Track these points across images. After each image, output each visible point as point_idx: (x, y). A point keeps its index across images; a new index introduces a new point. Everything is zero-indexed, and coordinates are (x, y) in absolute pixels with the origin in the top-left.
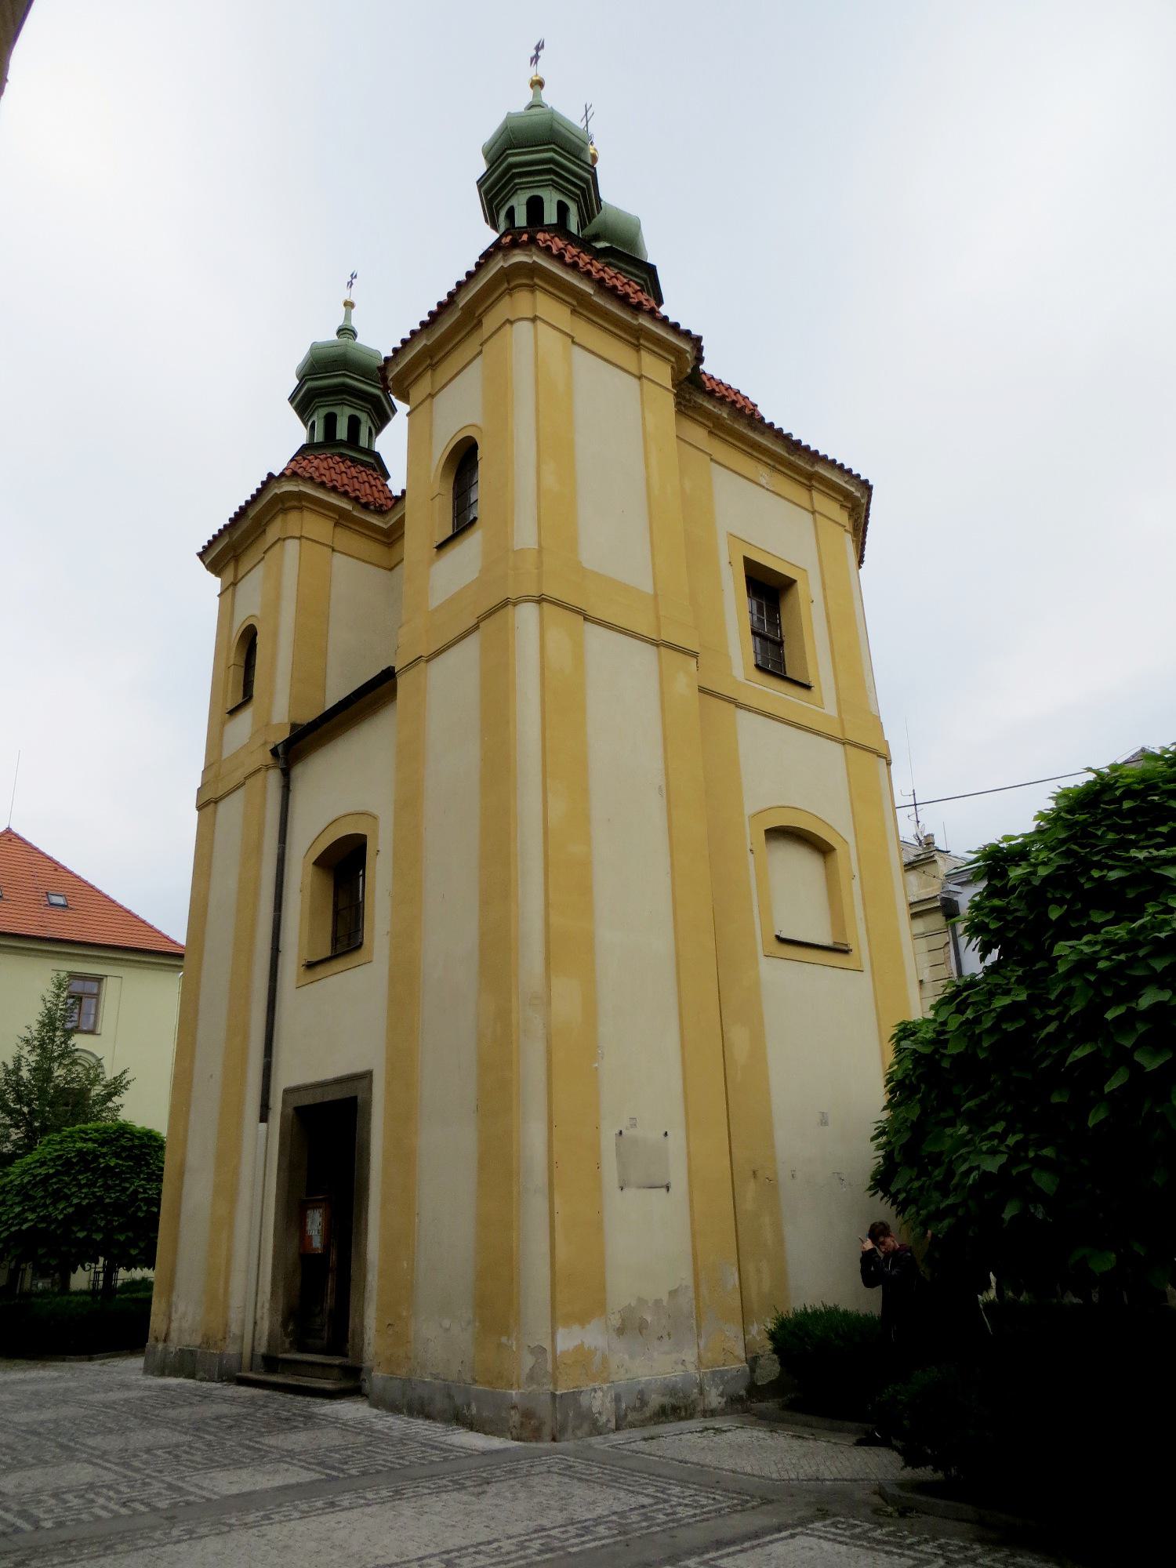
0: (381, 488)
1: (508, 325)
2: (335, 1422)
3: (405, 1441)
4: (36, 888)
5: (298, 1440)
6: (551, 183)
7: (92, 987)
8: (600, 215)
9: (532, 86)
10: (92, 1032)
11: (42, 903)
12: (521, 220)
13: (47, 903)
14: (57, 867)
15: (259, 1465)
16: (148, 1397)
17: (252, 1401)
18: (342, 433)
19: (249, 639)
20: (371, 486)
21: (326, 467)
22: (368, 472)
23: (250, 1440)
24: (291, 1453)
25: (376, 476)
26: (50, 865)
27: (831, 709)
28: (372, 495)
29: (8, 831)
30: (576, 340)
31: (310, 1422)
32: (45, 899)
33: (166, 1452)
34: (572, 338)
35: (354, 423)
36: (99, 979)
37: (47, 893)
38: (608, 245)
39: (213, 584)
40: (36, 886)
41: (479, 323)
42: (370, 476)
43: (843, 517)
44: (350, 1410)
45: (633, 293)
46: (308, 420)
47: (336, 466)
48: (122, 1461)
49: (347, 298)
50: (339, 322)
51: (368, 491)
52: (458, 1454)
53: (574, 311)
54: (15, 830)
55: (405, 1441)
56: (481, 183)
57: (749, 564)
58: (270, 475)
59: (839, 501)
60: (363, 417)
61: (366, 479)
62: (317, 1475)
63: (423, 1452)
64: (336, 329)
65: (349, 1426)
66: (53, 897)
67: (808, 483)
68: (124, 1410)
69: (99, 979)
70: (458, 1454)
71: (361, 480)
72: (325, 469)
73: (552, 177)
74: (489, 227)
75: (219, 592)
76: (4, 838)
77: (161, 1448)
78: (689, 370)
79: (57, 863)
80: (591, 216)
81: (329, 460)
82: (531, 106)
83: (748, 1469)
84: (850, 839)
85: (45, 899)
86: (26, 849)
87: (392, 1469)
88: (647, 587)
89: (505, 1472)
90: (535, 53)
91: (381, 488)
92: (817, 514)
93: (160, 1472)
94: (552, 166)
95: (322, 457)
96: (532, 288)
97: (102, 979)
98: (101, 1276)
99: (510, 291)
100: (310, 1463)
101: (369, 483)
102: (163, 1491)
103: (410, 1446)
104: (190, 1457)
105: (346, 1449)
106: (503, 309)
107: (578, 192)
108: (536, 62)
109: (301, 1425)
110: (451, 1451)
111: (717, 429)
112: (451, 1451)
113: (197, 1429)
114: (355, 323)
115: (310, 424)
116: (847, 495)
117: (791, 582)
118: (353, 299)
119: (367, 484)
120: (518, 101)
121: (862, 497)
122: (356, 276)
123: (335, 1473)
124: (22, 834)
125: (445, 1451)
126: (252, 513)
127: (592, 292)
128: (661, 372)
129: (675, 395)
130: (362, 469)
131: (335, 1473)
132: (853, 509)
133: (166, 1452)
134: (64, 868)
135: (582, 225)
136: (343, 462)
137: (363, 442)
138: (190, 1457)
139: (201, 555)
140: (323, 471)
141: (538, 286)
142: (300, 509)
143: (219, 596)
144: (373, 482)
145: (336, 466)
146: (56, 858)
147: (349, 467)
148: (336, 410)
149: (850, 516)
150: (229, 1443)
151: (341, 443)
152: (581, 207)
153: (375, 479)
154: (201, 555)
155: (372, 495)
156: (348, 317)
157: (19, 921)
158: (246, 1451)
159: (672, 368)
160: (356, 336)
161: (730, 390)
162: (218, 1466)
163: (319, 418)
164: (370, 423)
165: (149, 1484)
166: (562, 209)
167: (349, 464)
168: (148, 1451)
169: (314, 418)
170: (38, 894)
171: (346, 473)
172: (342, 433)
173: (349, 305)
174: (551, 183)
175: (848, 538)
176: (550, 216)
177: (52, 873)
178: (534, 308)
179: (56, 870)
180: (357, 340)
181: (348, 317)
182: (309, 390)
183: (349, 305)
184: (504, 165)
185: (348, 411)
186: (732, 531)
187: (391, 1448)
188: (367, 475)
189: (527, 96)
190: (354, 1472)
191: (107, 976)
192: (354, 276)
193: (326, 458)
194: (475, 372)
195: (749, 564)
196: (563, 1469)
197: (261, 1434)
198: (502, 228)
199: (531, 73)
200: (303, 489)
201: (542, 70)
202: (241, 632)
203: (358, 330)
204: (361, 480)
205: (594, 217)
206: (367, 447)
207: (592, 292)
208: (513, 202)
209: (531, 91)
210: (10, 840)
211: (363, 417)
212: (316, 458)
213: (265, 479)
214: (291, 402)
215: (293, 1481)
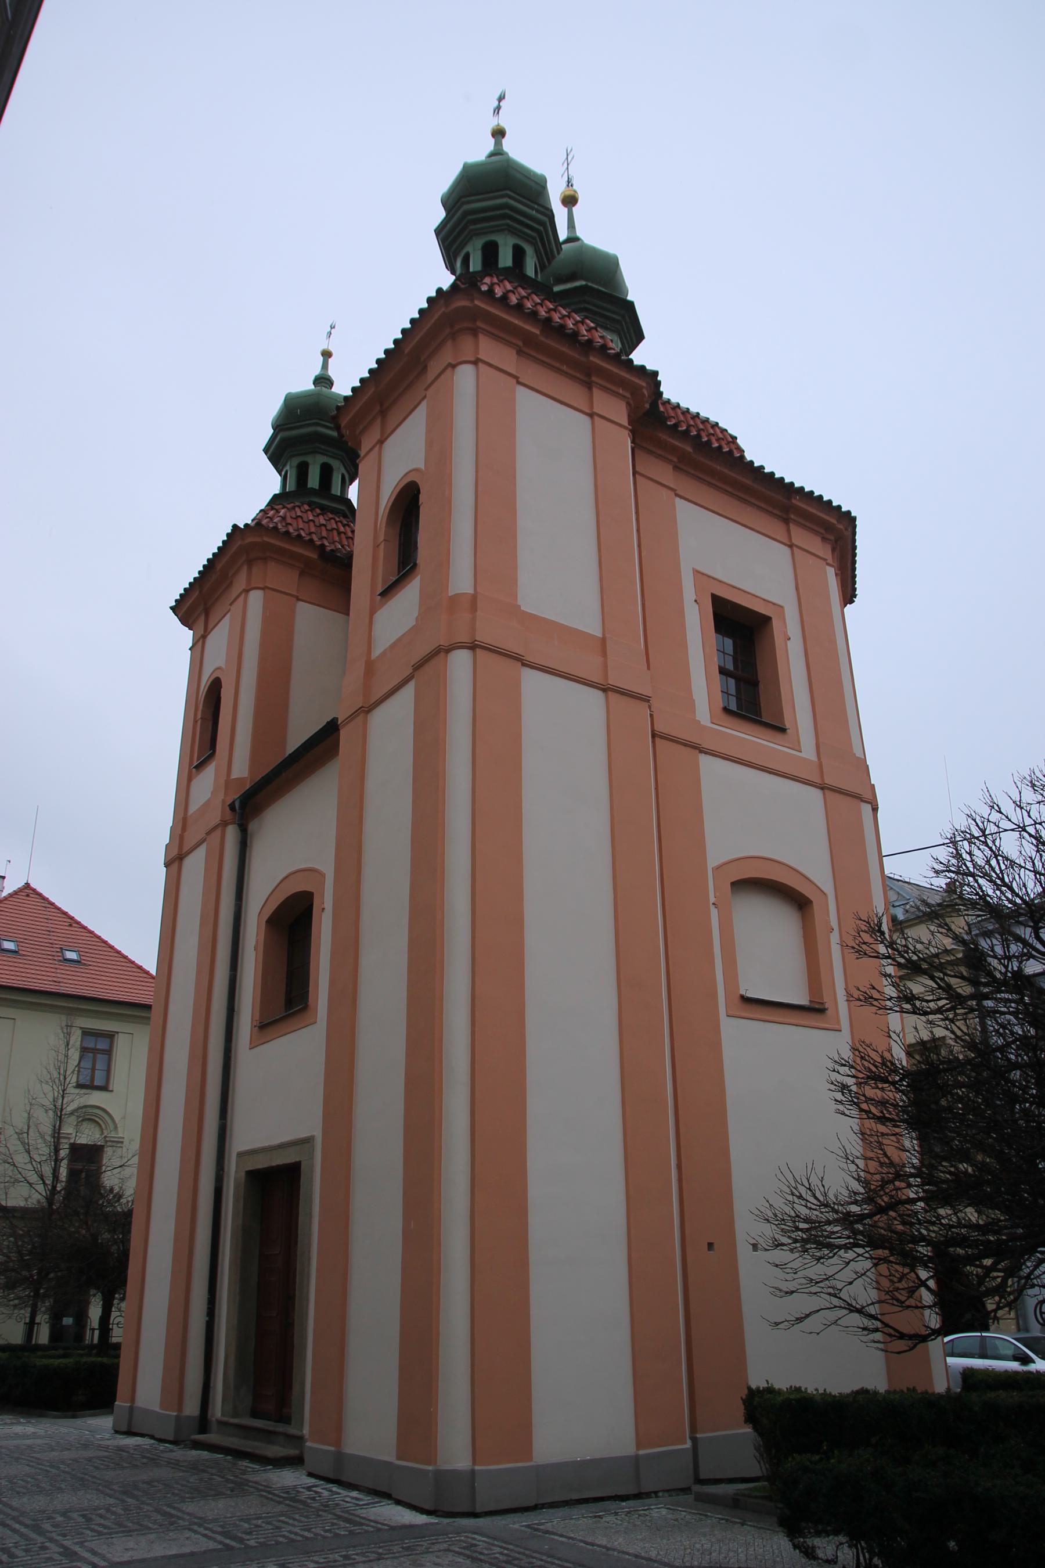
0: (350, 534)
1: (449, 370)
2: (267, 1492)
3: (320, 1513)
4: (51, 943)
5: (217, 1508)
6: (506, 227)
7: (102, 1045)
8: (560, 255)
9: (493, 135)
10: (104, 1088)
11: (56, 958)
12: (475, 264)
13: (61, 958)
14: (72, 922)
15: (163, 1532)
16: (98, 1458)
17: (195, 1467)
18: (314, 481)
19: (216, 686)
20: (339, 533)
21: (294, 516)
22: (338, 519)
23: (169, 1506)
24: (202, 1521)
25: (346, 523)
26: (65, 920)
27: (808, 751)
28: (340, 542)
29: (27, 885)
30: (520, 380)
31: (240, 1488)
32: (60, 954)
33: (81, 1515)
34: (516, 378)
35: (326, 473)
36: (111, 1036)
37: (61, 948)
38: (583, 283)
39: (186, 636)
40: (51, 941)
41: (425, 368)
42: (339, 524)
43: (824, 551)
44: (289, 1478)
45: (586, 330)
46: (282, 470)
47: (304, 516)
48: (35, 1523)
49: (325, 347)
50: (317, 371)
51: (337, 539)
52: (366, 1528)
53: (520, 352)
54: (33, 885)
55: (320, 1513)
56: (438, 232)
57: (716, 600)
58: (235, 527)
59: (821, 533)
60: (335, 464)
61: (335, 526)
62: (215, 1544)
63: (333, 1524)
64: (313, 378)
65: (275, 1495)
66: (67, 952)
67: (785, 516)
68: (67, 1469)
69: (111, 1036)
70: (366, 1528)
71: (329, 527)
72: (291, 517)
73: (508, 221)
74: (449, 272)
75: (191, 645)
76: (23, 894)
77: (78, 1511)
78: (647, 406)
79: (72, 918)
80: (550, 257)
81: (297, 509)
82: (492, 155)
83: (653, 1554)
84: (828, 887)
85: (60, 954)
86: (43, 905)
87: (293, 1541)
88: (592, 626)
89: (402, 1548)
90: (501, 104)
91: (350, 534)
92: (795, 548)
93: (64, 1535)
94: (507, 211)
95: (289, 506)
96: (475, 332)
97: (114, 1035)
98: (97, 1333)
99: (453, 336)
100: (214, 1532)
101: (337, 530)
102: (57, 1557)
103: (323, 1518)
104: (102, 1521)
105: (258, 1518)
106: (447, 355)
107: (534, 234)
108: (498, 113)
109: (229, 1492)
110: (362, 1524)
111: (684, 465)
112: (362, 1524)
113: (124, 1493)
114: (331, 373)
115: (283, 473)
116: (828, 528)
117: (767, 620)
118: (331, 349)
119: (335, 533)
120: (479, 151)
121: (846, 529)
122: (334, 327)
123: (233, 1543)
124: (40, 890)
125: (356, 1524)
126: (219, 566)
127: (538, 332)
128: (619, 412)
129: (630, 430)
130: (331, 516)
131: (233, 1543)
132: (836, 541)
133: (81, 1515)
134: (78, 923)
135: (541, 266)
136: (311, 511)
137: (336, 490)
138: (102, 1521)
139: (173, 609)
140: (289, 520)
141: (480, 328)
142: (265, 559)
143: (190, 649)
144: (342, 529)
145: (304, 516)
146: (72, 913)
147: (318, 515)
148: (308, 459)
149: (833, 550)
150: (146, 1508)
151: (313, 491)
152: (539, 249)
153: (344, 526)
154: (173, 609)
155: (340, 542)
156: (325, 366)
157: (28, 971)
158: (159, 1517)
159: (628, 404)
160: (332, 384)
161: (706, 423)
162: (123, 1532)
163: (291, 467)
164: (343, 470)
165: (46, 1548)
166: (519, 254)
167: (318, 511)
168: (64, 1514)
169: (288, 468)
170: (52, 949)
171: (302, 518)
172: (314, 481)
173: (327, 355)
174: (506, 227)
175: (831, 573)
176: (505, 259)
177: (67, 928)
178: (477, 353)
179: (71, 925)
180: (334, 389)
181: (325, 366)
182: (283, 440)
183: (327, 355)
184: (460, 212)
185: (321, 459)
186: (698, 568)
187: (303, 1519)
188: (336, 522)
189: (490, 145)
190: (252, 1543)
191: (118, 1033)
192: (332, 327)
193: (294, 508)
194: (420, 415)
195: (716, 600)
196: (464, 1548)
197: (183, 1500)
198: (458, 272)
199: (492, 123)
200: (266, 539)
201: (504, 121)
202: (209, 682)
203: (333, 378)
204: (317, 524)
205: (553, 257)
206: (339, 494)
207: (538, 332)
208: (469, 248)
209: (492, 141)
210: (28, 896)
211: (335, 464)
212: (284, 507)
213: (230, 531)
214: (266, 453)
215: (186, 1550)
